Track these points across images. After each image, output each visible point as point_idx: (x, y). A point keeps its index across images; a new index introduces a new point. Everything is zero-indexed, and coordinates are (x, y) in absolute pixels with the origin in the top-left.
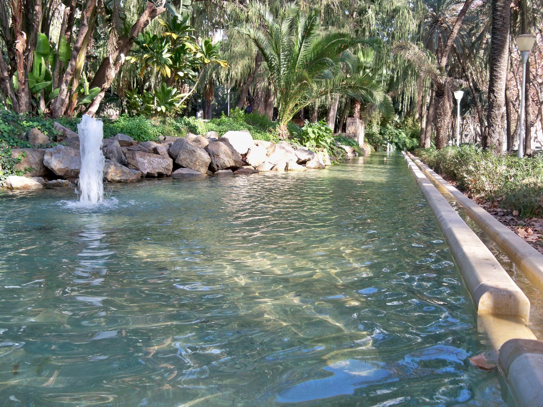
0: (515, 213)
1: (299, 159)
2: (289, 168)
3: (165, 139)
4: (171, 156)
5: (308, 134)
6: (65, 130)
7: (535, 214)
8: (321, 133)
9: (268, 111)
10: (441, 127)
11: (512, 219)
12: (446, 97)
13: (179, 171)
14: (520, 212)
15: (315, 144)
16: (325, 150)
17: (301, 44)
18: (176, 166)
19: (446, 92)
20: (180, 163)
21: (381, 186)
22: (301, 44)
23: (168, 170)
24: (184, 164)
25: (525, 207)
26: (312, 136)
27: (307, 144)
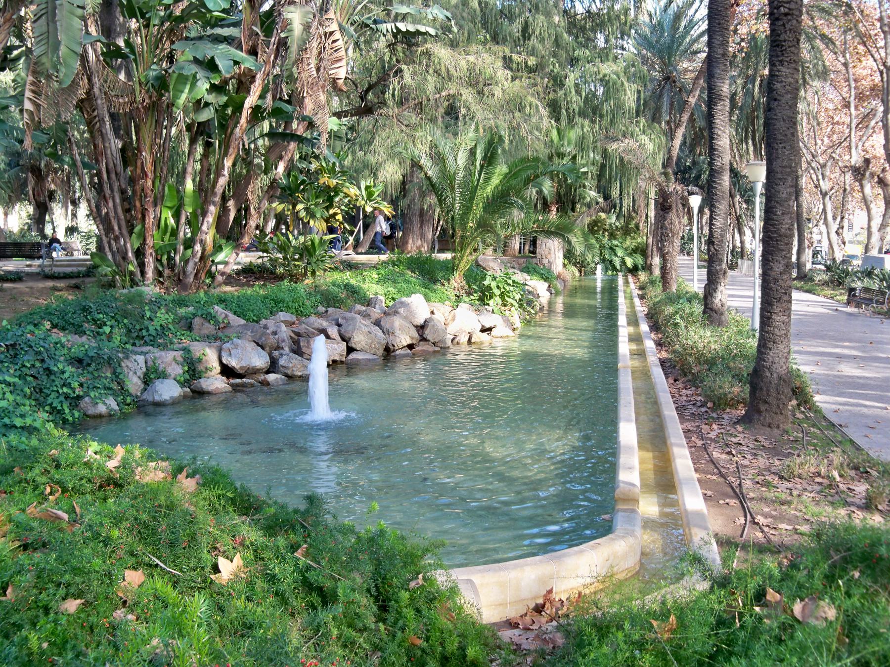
0: (710, 405)
1: (483, 326)
2: (473, 341)
3: (327, 311)
4: (343, 339)
5: (491, 289)
6: (226, 316)
7: (729, 405)
8: (507, 288)
9: (425, 229)
10: (667, 253)
11: (706, 412)
12: (674, 211)
13: (353, 356)
14: (714, 404)
15: (500, 302)
16: (513, 309)
17: (480, 174)
18: (350, 350)
19: (674, 206)
20: (354, 346)
21: (582, 364)
22: (480, 174)
23: (341, 355)
24: (358, 347)
25: (720, 399)
26: (497, 292)
27: (491, 302)
